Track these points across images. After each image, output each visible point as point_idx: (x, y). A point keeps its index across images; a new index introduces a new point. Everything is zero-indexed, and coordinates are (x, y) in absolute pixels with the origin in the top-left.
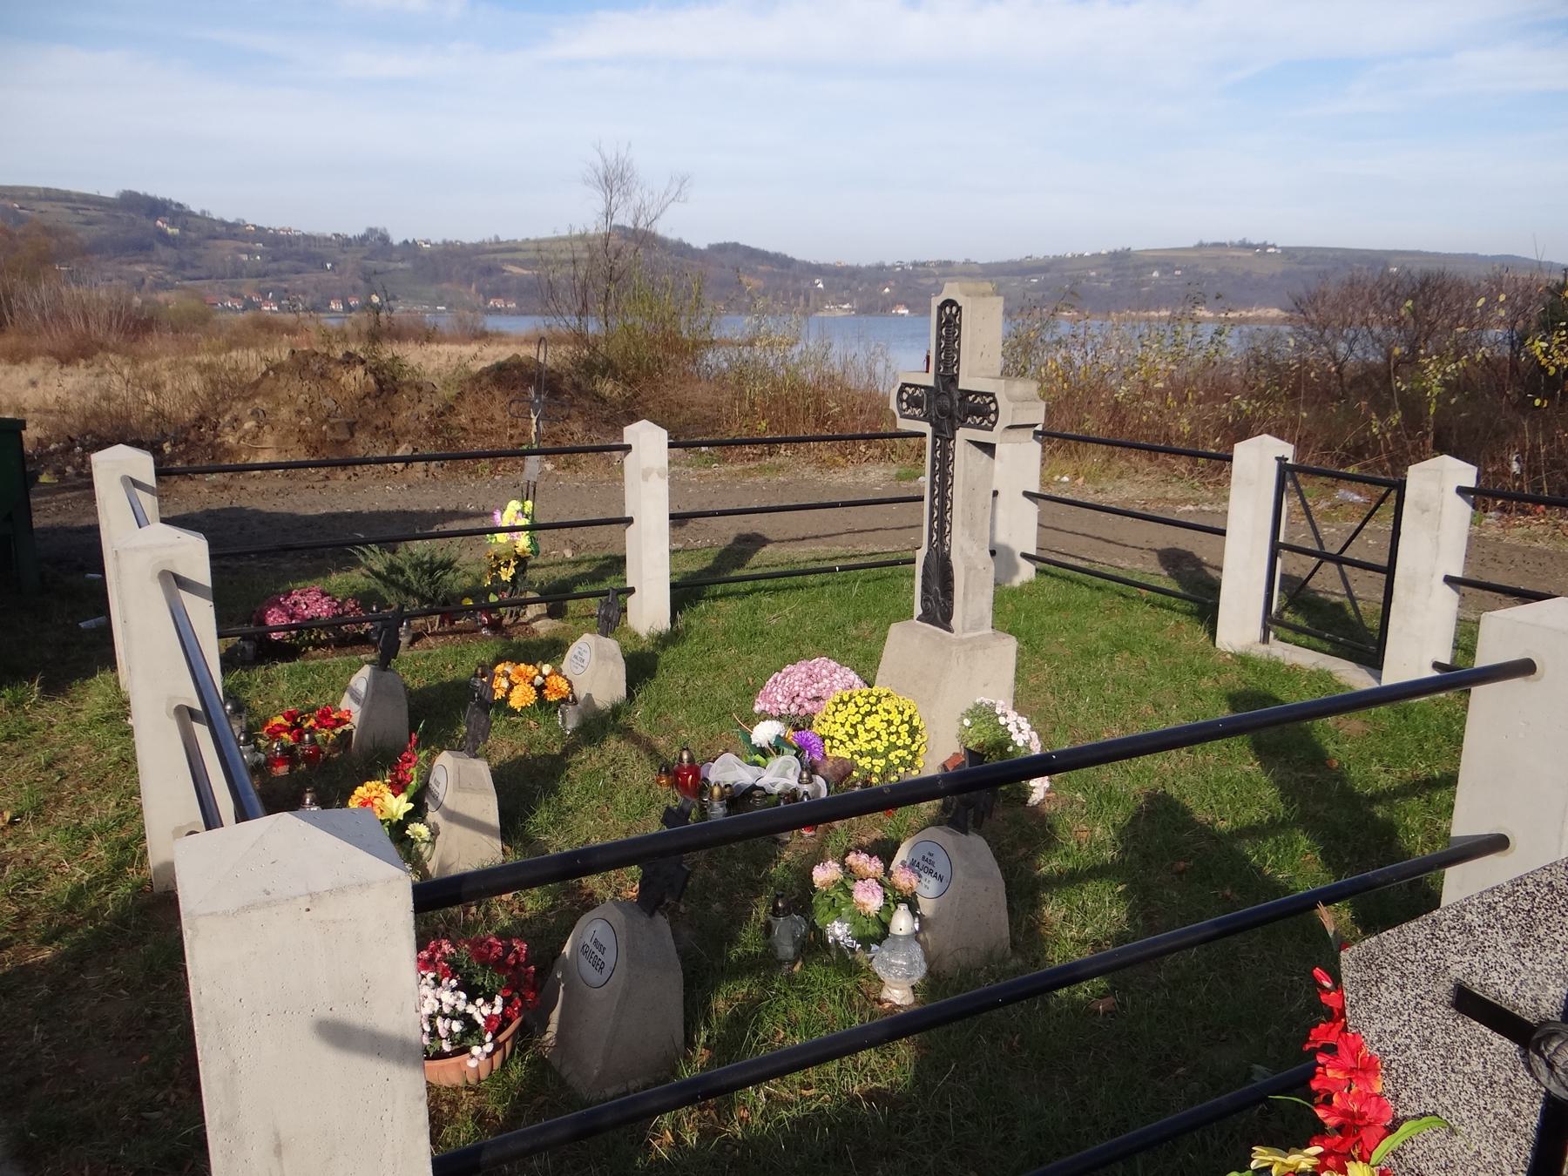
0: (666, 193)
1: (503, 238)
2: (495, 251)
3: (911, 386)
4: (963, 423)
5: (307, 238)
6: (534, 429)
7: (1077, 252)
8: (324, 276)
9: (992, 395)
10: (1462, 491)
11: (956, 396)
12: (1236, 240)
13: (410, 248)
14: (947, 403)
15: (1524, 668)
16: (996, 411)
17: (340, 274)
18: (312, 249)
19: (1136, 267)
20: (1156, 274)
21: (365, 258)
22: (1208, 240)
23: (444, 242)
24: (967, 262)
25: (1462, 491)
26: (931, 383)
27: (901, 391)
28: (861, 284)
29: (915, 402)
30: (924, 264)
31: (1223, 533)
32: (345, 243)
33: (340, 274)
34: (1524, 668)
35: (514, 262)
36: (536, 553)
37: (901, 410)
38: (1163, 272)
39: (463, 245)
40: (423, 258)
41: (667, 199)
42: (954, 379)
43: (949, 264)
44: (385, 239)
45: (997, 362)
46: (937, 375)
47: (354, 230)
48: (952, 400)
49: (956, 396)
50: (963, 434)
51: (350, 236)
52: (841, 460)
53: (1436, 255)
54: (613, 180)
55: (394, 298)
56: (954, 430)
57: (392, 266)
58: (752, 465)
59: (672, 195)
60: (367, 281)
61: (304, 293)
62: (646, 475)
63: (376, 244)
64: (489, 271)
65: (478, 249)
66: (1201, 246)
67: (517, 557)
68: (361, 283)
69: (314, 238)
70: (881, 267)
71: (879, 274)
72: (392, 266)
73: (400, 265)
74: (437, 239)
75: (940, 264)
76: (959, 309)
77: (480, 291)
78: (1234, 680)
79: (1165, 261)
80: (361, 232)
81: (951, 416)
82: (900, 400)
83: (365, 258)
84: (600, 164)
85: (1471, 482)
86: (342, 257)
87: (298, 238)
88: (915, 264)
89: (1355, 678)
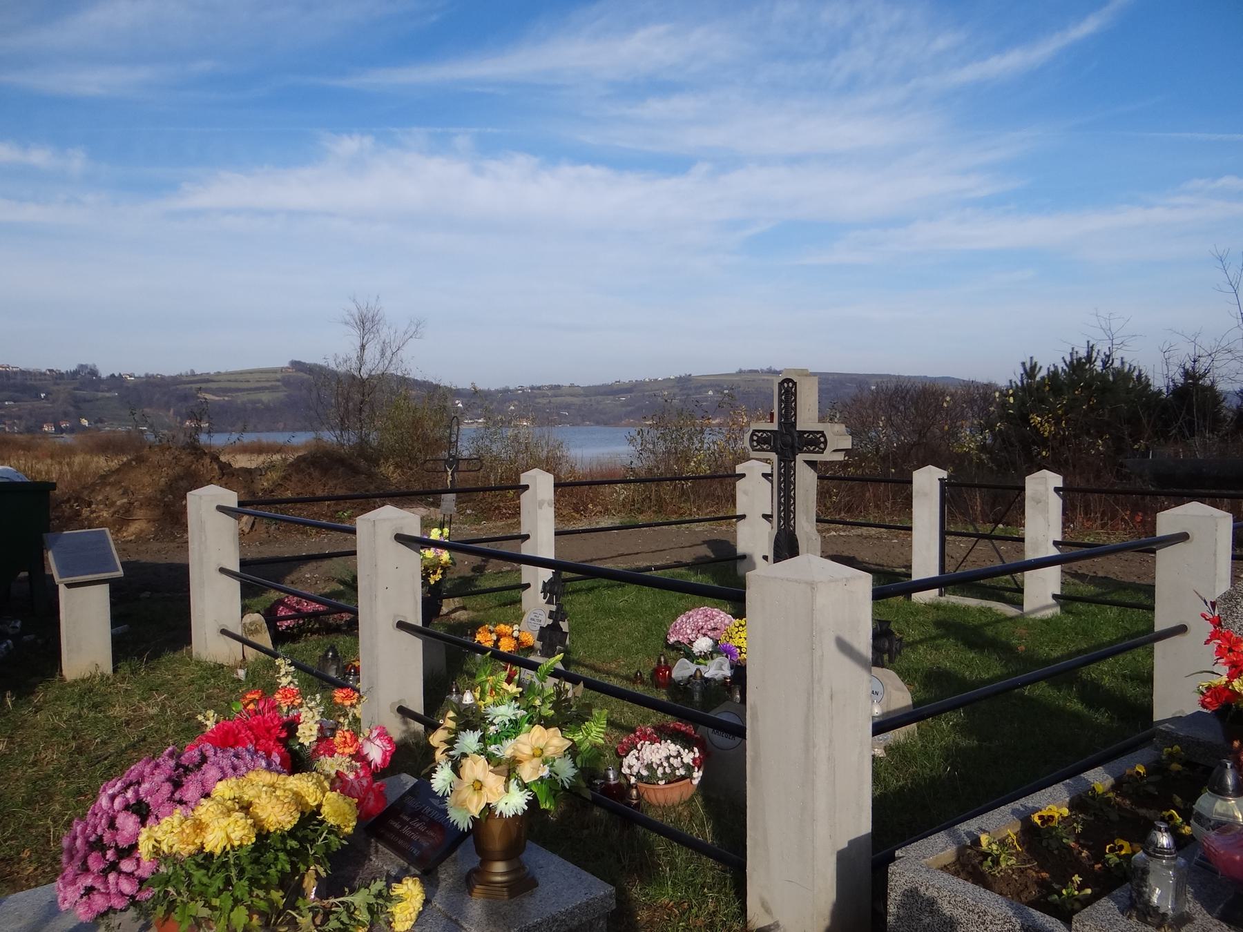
0: (406, 333)
1: (198, 372)
2: (191, 382)
3: (759, 431)
4: (801, 451)
5: (23, 373)
6: (450, 478)
7: (653, 378)
8: (37, 404)
9: (822, 432)
10: (1057, 490)
11: (796, 435)
12: (765, 368)
13: (116, 381)
14: (789, 439)
15: (1183, 537)
16: (825, 442)
17: (54, 402)
18: (29, 382)
19: (696, 388)
20: (710, 393)
21: (75, 389)
22: (746, 368)
23: (147, 376)
24: (572, 386)
25: (1057, 490)
26: (776, 428)
27: (753, 434)
28: (491, 403)
29: (761, 441)
30: (539, 388)
31: (910, 529)
32: (58, 377)
33: (54, 402)
34: (1183, 537)
35: (207, 391)
36: (454, 564)
37: (752, 446)
38: (716, 391)
39: (163, 378)
40: (128, 388)
41: (407, 336)
42: (794, 424)
43: (558, 387)
44: (93, 372)
45: (816, 414)
46: (780, 424)
47: (66, 365)
48: (793, 438)
49: (796, 435)
50: (800, 458)
51: (63, 371)
52: (577, 516)
53: (909, 378)
54: (366, 323)
55: (102, 421)
56: (794, 455)
57: (100, 395)
58: (510, 521)
59: (411, 333)
60: (78, 408)
61: (20, 418)
62: (541, 505)
63: (86, 378)
64: (185, 398)
65: (176, 380)
66: (741, 372)
67: (442, 568)
68: (71, 409)
69: (30, 373)
70: (506, 391)
71: (506, 395)
72: (100, 395)
73: (108, 395)
74: (140, 373)
75: (552, 388)
76: (795, 384)
77: (177, 413)
78: (932, 616)
79: (716, 383)
80: (73, 368)
81: (792, 447)
82: (752, 440)
83: (75, 389)
84: (355, 311)
85: (1060, 485)
86: (55, 388)
87: (15, 373)
88: (532, 388)
89: (1010, 611)
